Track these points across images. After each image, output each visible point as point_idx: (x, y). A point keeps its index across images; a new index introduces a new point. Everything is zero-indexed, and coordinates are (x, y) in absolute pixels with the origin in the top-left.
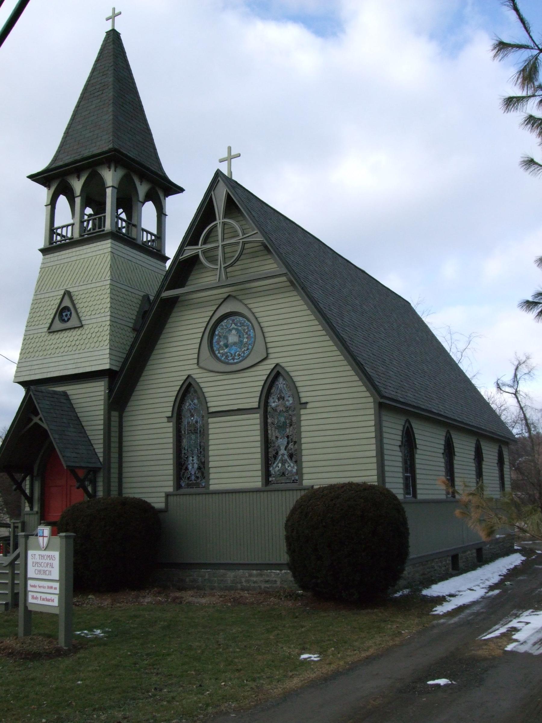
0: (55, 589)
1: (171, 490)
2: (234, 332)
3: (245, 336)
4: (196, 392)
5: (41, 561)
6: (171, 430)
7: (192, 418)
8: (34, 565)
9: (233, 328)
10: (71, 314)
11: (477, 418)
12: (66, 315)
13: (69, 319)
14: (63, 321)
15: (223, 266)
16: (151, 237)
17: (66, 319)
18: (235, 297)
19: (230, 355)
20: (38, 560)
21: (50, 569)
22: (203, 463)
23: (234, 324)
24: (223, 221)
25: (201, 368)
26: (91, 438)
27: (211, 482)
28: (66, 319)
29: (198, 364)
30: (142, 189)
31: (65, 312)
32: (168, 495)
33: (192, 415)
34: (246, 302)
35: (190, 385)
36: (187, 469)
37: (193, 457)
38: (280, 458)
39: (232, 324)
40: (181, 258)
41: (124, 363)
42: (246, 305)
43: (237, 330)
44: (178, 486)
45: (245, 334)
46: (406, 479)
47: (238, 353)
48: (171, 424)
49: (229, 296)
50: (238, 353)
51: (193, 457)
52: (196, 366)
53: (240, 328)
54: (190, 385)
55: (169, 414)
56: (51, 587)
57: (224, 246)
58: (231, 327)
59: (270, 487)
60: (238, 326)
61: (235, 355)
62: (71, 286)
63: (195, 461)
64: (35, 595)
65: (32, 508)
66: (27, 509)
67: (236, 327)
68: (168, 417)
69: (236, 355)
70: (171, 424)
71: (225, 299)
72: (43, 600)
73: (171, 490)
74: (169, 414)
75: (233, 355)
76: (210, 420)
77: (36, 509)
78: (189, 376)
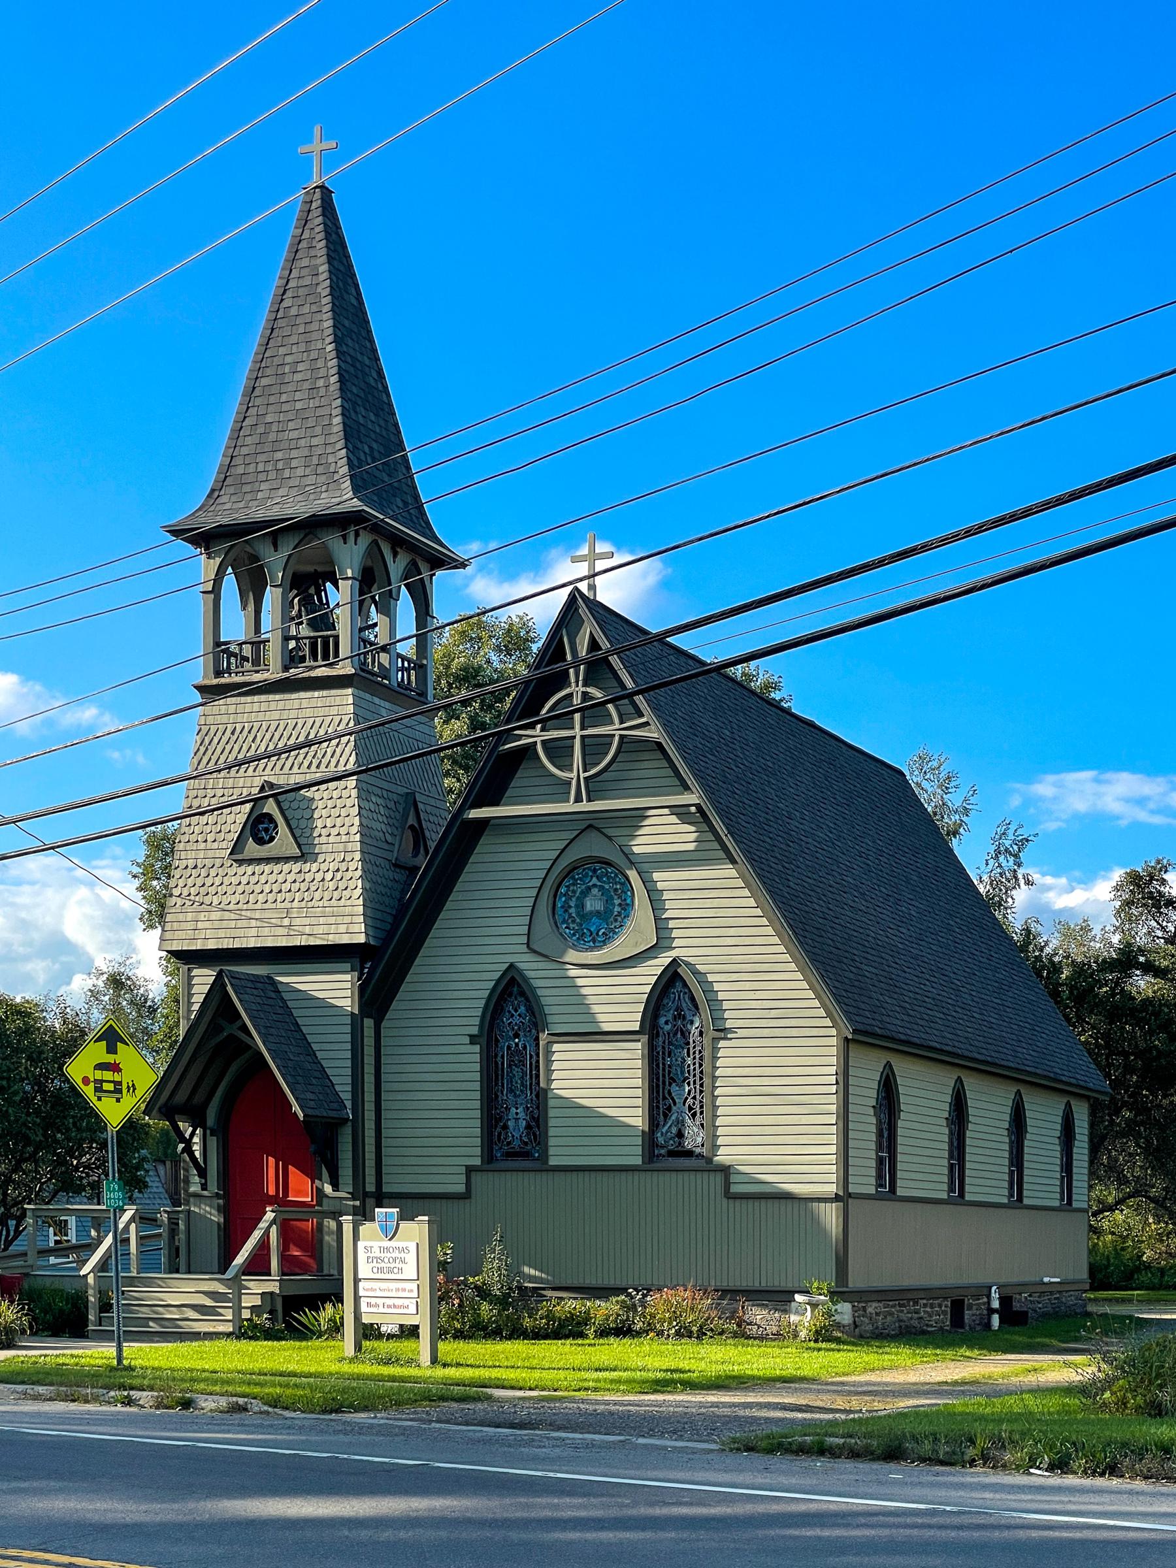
0: (412, 1291)
1: (477, 1162)
2: (595, 891)
3: (617, 902)
4: (522, 993)
5: (382, 1255)
6: (477, 1058)
7: (517, 1040)
8: (370, 1260)
9: (595, 886)
10: (276, 826)
11: (1019, 1049)
12: (266, 830)
13: (272, 839)
14: (260, 841)
15: (582, 776)
16: (403, 664)
17: (267, 838)
18: (598, 829)
19: (588, 934)
20: (378, 1254)
21: (400, 1266)
22: (537, 1120)
23: (597, 877)
24: (584, 689)
25: (535, 952)
26: (325, 1064)
27: (551, 1151)
28: (267, 838)
29: (528, 944)
30: (396, 566)
31: (263, 823)
32: (470, 1170)
33: (516, 1036)
34: (610, 832)
35: (513, 981)
36: (505, 1127)
37: (517, 1108)
38: (673, 1118)
39: (592, 877)
40: (501, 748)
41: (390, 934)
42: (610, 838)
43: (601, 888)
44: (489, 1157)
45: (616, 897)
46: (880, 1161)
47: (603, 930)
48: (477, 1048)
49: (590, 826)
50: (603, 930)
51: (517, 1108)
52: (524, 948)
53: (607, 887)
54: (513, 981)
55: (475, 1031)
56: (404, 1290)
57: (583, 737)
58: (590, 884)
59: (492, 1166)
60: (604, 882)
61: (597, 934)
62: (273, 773)
63: (522, 1115)
64: (373, 1301)
65: (204, 1187)
66: (195, 1188)
67: (599, 884)
68: (470, 1036)
69: (600, 933)
70: (477, 1048)
71: (583, 831)
72: (389, 1307)
73: (477, 1162)
74: (475, 1031)
75: (594, 934)
76: (556, 1047)
77: (213, 1187)
78: (512, 966)
